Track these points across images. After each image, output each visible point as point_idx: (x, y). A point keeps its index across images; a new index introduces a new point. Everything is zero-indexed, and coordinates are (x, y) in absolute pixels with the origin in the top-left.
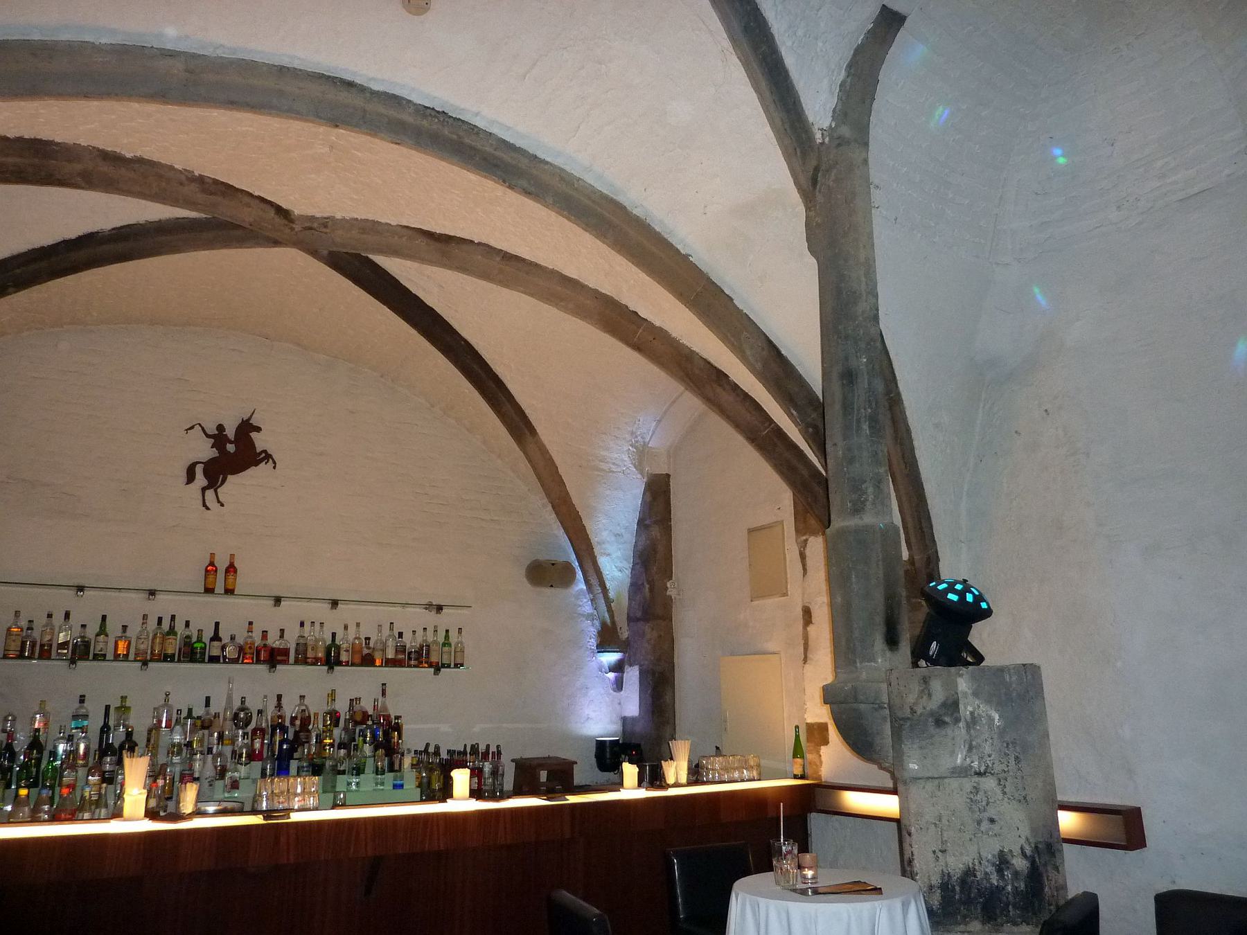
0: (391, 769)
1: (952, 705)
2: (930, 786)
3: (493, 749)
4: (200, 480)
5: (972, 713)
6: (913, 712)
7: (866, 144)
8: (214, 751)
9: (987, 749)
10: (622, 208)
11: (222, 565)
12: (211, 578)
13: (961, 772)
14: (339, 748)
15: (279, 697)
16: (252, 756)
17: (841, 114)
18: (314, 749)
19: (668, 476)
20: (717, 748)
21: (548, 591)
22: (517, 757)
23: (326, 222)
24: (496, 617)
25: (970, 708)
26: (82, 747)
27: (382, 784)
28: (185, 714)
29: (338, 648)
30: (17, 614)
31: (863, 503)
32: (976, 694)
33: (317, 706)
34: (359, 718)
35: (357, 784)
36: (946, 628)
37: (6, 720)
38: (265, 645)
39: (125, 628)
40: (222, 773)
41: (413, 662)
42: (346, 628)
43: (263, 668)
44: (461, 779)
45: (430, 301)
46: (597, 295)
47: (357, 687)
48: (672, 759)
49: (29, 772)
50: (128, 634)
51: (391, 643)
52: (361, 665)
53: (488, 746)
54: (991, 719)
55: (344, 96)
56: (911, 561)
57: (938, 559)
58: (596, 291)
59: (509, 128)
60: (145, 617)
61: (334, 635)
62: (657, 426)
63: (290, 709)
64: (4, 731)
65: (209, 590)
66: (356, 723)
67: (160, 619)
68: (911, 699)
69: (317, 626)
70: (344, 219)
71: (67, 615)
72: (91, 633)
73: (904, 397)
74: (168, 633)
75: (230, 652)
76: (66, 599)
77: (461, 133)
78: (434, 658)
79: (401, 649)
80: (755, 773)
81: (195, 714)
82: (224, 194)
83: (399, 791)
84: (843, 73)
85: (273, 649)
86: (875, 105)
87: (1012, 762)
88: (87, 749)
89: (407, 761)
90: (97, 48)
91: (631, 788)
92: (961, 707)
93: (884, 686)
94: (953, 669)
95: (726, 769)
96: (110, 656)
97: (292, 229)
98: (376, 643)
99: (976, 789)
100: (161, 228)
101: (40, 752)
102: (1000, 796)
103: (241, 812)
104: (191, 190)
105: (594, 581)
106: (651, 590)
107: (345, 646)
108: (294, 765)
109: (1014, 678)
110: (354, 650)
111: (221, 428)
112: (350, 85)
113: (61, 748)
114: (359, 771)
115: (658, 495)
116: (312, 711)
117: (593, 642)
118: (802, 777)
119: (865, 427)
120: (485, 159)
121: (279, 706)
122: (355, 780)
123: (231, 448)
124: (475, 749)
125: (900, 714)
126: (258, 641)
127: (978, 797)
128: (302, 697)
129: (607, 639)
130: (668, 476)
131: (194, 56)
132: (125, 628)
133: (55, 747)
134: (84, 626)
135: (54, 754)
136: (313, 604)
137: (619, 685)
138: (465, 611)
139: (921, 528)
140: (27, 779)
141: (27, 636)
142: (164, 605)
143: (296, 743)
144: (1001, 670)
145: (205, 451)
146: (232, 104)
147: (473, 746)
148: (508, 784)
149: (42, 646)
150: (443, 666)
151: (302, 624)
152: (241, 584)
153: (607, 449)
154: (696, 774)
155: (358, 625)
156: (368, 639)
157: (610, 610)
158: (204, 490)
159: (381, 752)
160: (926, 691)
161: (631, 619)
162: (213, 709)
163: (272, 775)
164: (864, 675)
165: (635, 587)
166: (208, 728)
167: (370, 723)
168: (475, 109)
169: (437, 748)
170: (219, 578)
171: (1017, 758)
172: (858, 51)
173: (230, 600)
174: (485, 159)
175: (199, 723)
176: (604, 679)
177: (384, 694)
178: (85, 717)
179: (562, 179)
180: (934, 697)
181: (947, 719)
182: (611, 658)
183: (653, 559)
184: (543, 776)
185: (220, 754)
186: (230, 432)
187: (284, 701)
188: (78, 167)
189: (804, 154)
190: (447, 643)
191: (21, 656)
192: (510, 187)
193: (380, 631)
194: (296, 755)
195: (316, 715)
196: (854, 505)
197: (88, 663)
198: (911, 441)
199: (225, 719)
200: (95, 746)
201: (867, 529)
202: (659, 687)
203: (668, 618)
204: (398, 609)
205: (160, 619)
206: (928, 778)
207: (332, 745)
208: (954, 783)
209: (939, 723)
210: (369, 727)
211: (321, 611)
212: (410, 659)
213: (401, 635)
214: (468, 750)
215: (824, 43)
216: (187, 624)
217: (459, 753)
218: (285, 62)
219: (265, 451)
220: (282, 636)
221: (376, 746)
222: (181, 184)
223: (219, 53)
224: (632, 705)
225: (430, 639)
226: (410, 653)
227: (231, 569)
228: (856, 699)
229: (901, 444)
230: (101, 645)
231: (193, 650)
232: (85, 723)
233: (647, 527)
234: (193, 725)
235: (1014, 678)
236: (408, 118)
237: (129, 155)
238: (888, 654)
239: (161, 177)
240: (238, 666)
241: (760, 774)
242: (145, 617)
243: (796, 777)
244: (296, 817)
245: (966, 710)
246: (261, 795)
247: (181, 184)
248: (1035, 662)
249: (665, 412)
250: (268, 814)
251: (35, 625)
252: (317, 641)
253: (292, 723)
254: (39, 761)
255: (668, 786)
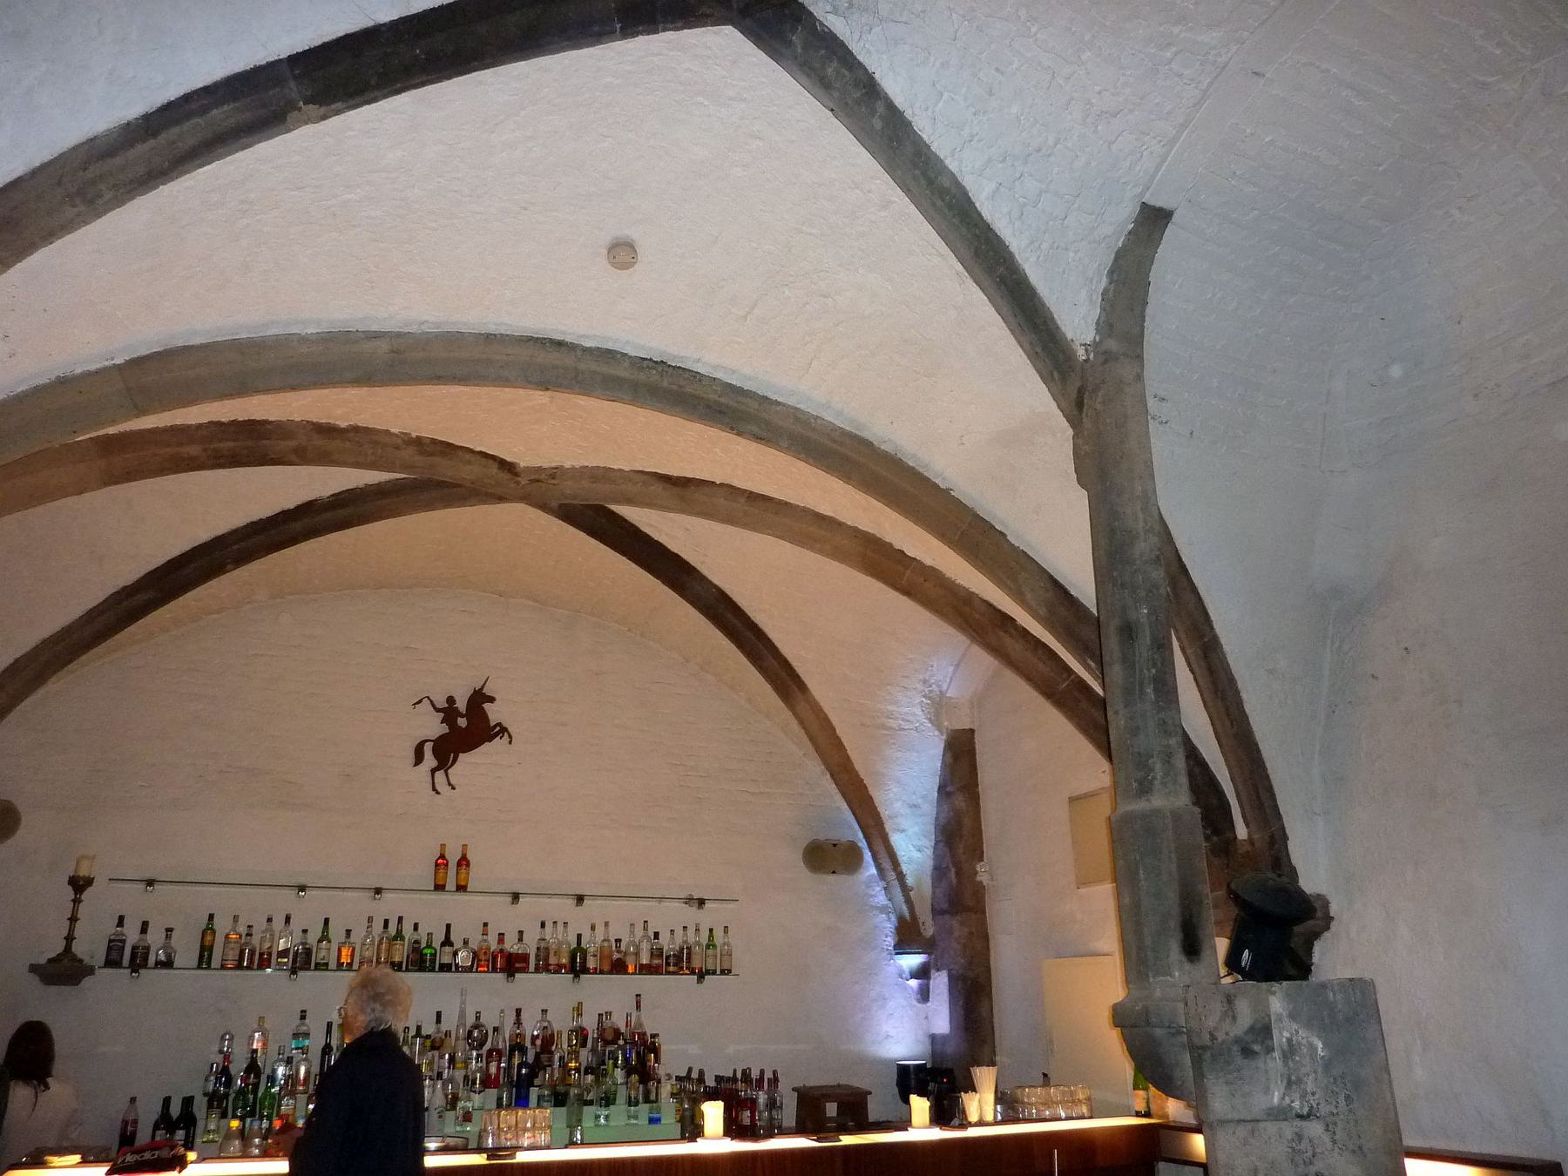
0: (647, 1100)
1: (1263, 1031)
2: (1242, 1131)
3: (768, 1075)
4: (430, 761)
5: (1289, 1040)
6: (1213, 1038)
7: (1140, 358)
8: (445, 1076)
9: (1310, 1087)
10: (868, 444)
11: (453, 857)
12: (209, 938)
13: (1279, 1114)
14: (586, 1073)
15: (518, 1012)
16: (487, 1082)
17: (1106, 326)
18: (556, 1075)
19: (972, 731)
20: (1045, 1075)
21: (832, 878)
22: (799, 1084)
23: (555, 473)
24: (768, 912)
25: (1286, 1034)
26: (303, 1070)
27: (636, 1117)
28: (413, 1032)
29: (584, 953)
30: (236, 918)
31: (1151, 782)
32: (1293, 1016)
33: (561, 1023)
34: (609, 1036)
35: (607, 1117)
36: (1278, 932)
37: (223, 1039)
38: (502, 951)
39: (348, 932)
40: (453, 1102)
41: (671, 969)
42: (593, 928)
43: (500, 976)
44: (713, 1113)
45: (674, 547)
46: (856, 533)
47: (606, 999)
48: (974, 1090)
49: (245, 1100)
50: (352, 940)
51: (645, 946)
52: (611, 972)
53: (762, 1072)
54: (1312, 1048)
55: (554, 358)
56: (1251, 841)
57: (1285, 838)
58: (856, 529)
59: (734, 372)
60: (370, 920)
61: (579, 936)
62: (955, 672)
63: (531, 1028)
64: (221, 1052)
65: (439, 887)
66: (607, 1043)
67: (386, 922)
68: (1211, 1023)
69: (560, 927)
70: (573, 468)
71: (288, 919)
72: (312, 938)
73: (1223, 641)
74: (395, 938)
75: (463, 957)
76: (286, 901)
77: (682, 383)
78: (697, 963)
79: (657, 953)
80: (1085, 1110)
81: (424, 1033)
82: (443, 454)
83: (654, 1127)
84: (1105, 280)
85: (510, 955)
86: (1149, 311)
87: (1342, 1103)
88: (308, 1073)
89: (666, 1089)
90: (303, 339)
91: (921, 1128)
92: (1275, 1033)
93: (1182, 1005)
94: (1264, 985)
95: (1048, 1103)
96: (333, 965)
97: (518, 483)
98: (628, 947)
99: (1299, 1137)
100: (380, 491)
101: (258, 1076)
102: (1329, 1145)
103: (465, 1150)
104: (408, 454)
105: (887, 865)
106: (958, 874)
107: (592, 950)
108: (534, 1093)
109: (1339, 997)
110: (602, 954)
111: (451, 700)
112: (560, 344)
113: (281, 1071)
114: (608, 1100)
115: (961, 755)
116: (556, 1027)
117: (890, 941)
118: (1147, 1115)
119: (1149, 690)
120: (709, 407)
121: (518, 1022)
122: (604, 1112)
123: (462, 722)
124: (746, 1075)
125: (1196, 1041)
126: (494, 946)
127: (1302, 1147)
128: (544, 1011)
129: (907, 937)
130: (972, 731)
131: (399, 335)
132: (348, 932)
133: (274, 1071)
134: (305, 931)
135: (272, 1079)
136: (555, 900)
137: (924, 995)
138: (732, 906)
139: (1259, 797)
140: (244, 1108)
141: (246, 944)
142: (390, 906)
143: (536, 1068)
144: (1324, 986)
145: (435, 727)
146: (438, 379)
147: (744, 1072)
148: (789, 1116)
149: (261, 954)
150: (708, 972)
151: (543, 925)
152: (476, 878)
153: (896, 703)
154: (1010, 1106)
155: (607, 924)
156: (618, 941)
157: (908, 901)
158: (433, 771)
159: (635, 1078)
160: (1231, 1014)
161: (936, 912)
162: (444, 1027)
163: (509, 1106)
164: (1158, 993)
165: (939, 872)
166: (438, 1048)
167: (621, 1042)
168: (696, 356)
169: (701, 1073)
170: (450, 873)
171: (1348, 1098)
172: (1120, 255)
173: (461, 897)
174: (709, 407)
175: (428, 1043)
176: (906, 988)
177: (638, 1007)
178: (306, 1035)
179: (797, 419)
180: (1240, 1021)
181: (1257, 1048)
182: (913, 961)
183: (960, 835)
184: (831, 1109)
185: (451, 1080)
186: (461, 705)
187: (524, 1016)
188: (292, 443)
189: (1064, 379)
190: (711, 944)
191: (239, 966)
192: (739, 434)
193: (632, 932)
194: (537, 1082)
195: (560, 1033)
196: (1140, 784)
197: (309, 973)
198: (1237, 692)
199: (457, 1039)
200: (316, 1069)
201: (1156, 812)
202: (973, 996)
203: (984, 912)
204: (653, 903)
205: (386, 922)
206: (1240, 1121)
207: (577, 1070)
208: (1271, 1128)
209: (1247, 1052)
210: (620, 1047)
211: (563, 908)
212: (668, 964)
213: (656, 935)
214: (739, 1075)
215: (1076, 252)
216: (416, 927)
217: (728, 1079)
218: (492, 329)
219: (499, 724)
220: (520, 940)
221: (629, 1070)
222: (397, 448)
223: (425, 328)
224: (941, 1019)
225: (691, 938)
226: (668, 957)
227: (464, 862)
228: (1148, 1023)
229: (1223, 699)
230: (323, 953)
231: (423, 956)
232: (307, 1042)
233: (949, 794)
234: (422, 1044)
235: (1339, 997)
236: (622, 372)
237: (343, 425)
238: (1187, 966)
239: (376, 443)
240: (472, 975)
241: (1091, 1110)
242: (370, 920)
243: (1138, 1114)
244: (522, 1157)
245: (1280, 1036)
246: (485, 1130)
247: (397, 448)
248: (1367, 976)
249: (964, 655)
250: (492, 1153)
251: (254, 931)
252: (560, 943)
253: (533, 1043)
254: (256, 1086)
255: (964, 1125)
